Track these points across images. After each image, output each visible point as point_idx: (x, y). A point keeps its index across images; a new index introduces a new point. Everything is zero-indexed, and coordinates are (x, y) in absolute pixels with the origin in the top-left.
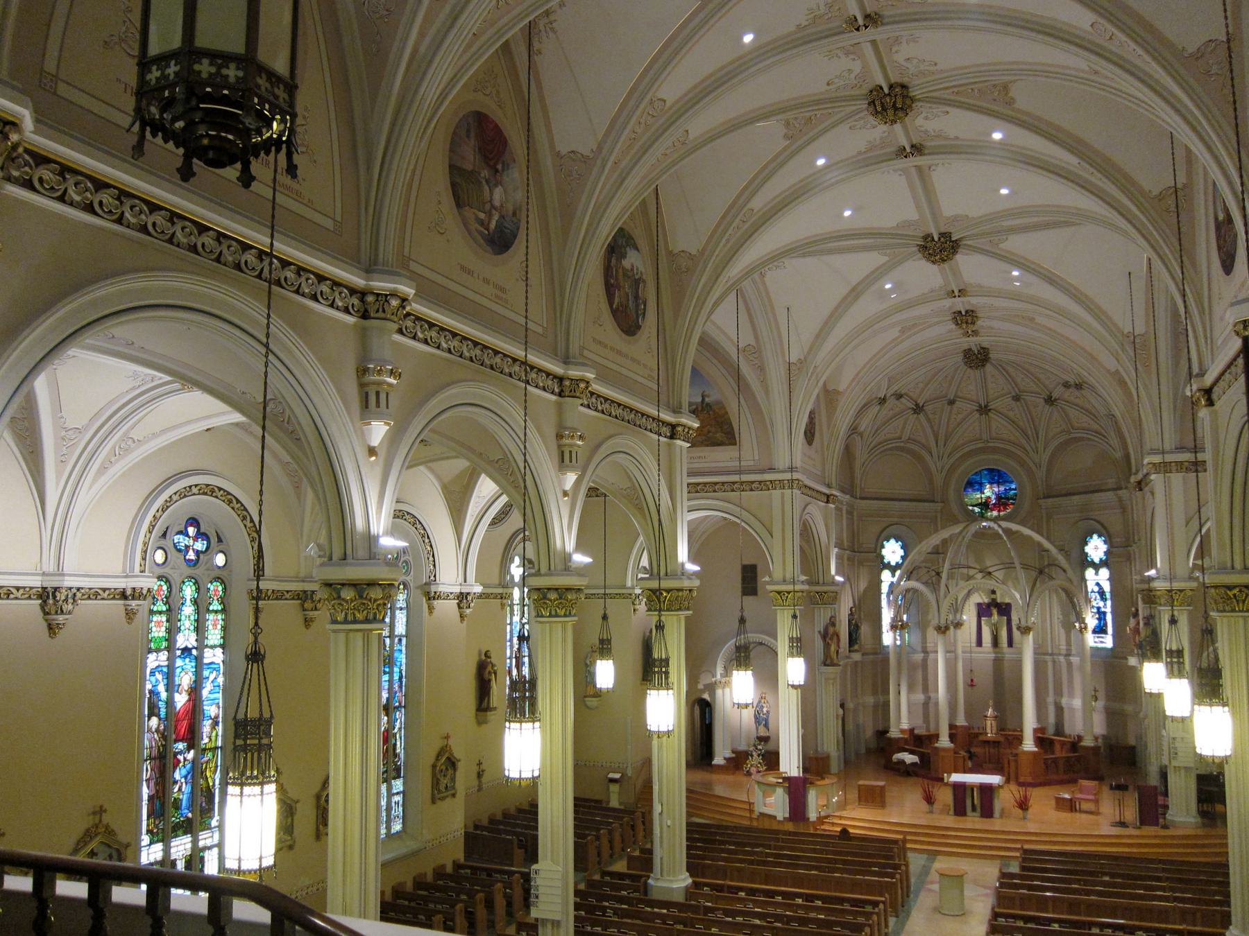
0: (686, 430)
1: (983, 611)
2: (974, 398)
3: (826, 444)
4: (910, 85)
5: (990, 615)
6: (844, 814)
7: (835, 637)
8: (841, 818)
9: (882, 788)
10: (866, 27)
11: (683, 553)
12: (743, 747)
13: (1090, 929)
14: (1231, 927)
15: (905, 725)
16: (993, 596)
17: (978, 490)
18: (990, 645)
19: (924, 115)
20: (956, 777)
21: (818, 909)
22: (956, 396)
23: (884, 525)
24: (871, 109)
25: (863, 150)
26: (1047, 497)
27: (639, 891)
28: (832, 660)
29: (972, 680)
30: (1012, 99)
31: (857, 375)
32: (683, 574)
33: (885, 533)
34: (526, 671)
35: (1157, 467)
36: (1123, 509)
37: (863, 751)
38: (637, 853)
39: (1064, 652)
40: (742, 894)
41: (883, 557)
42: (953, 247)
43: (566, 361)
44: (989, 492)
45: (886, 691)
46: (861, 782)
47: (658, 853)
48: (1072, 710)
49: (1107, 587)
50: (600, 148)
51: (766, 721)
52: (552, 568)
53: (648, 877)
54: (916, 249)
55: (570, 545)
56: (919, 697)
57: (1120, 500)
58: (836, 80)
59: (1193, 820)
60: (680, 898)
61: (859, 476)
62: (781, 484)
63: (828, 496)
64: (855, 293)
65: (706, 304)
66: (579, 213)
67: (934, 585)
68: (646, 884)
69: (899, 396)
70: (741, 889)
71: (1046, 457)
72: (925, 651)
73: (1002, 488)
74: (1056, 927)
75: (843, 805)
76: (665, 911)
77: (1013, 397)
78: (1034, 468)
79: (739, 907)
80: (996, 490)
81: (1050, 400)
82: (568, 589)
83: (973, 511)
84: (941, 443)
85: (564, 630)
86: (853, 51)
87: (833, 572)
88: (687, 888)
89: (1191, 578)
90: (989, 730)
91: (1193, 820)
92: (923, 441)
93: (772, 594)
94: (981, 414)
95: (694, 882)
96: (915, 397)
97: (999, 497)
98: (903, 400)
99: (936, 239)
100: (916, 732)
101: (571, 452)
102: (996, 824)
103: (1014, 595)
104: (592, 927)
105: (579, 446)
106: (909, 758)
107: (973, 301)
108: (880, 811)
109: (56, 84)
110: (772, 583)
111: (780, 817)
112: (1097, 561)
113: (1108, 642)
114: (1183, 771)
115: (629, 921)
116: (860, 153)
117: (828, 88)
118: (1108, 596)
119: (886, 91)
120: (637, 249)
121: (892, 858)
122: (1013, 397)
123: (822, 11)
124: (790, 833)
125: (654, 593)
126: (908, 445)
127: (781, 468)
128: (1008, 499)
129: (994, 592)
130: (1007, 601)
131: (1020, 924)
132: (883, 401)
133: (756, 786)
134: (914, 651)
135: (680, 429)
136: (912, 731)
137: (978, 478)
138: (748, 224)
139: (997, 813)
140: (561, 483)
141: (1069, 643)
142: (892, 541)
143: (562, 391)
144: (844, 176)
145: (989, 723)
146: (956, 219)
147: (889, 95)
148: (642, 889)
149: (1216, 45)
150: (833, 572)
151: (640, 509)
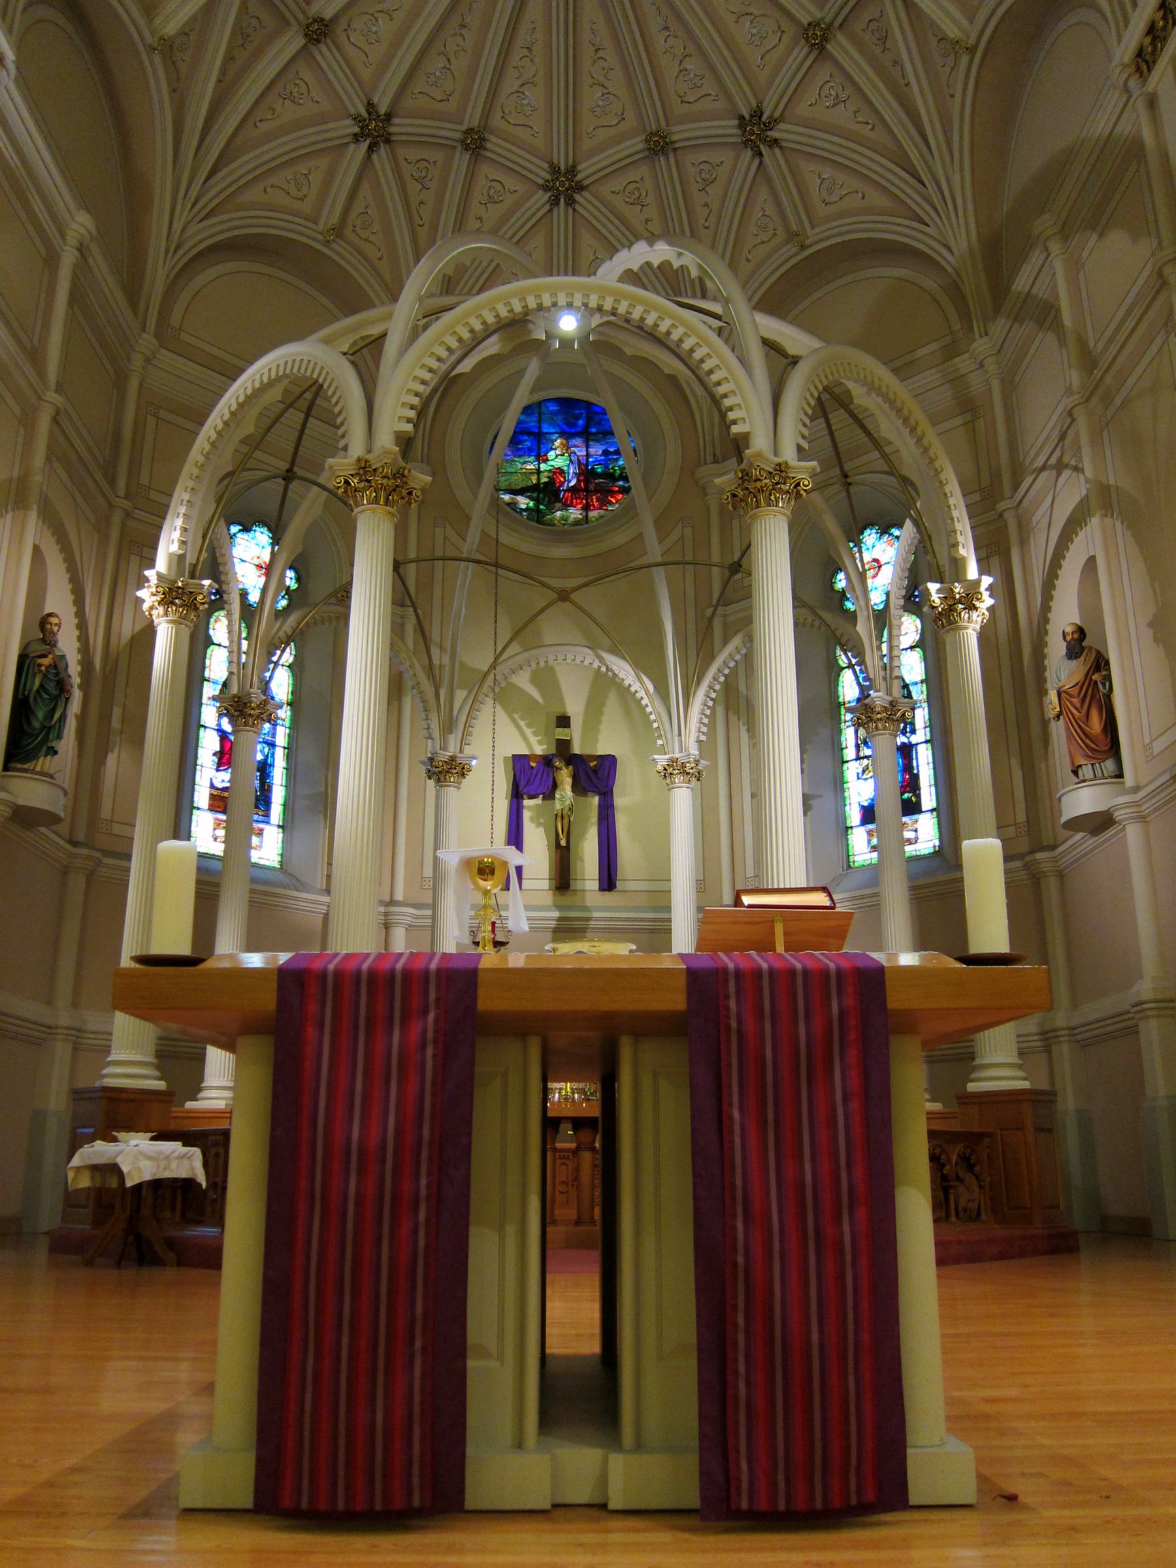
16: (561, 734)
17: (529, 452)
18: (545, 884)
83: (513, 505)
96: (690, 158)
97: (586, 473)
128: (612, 477)
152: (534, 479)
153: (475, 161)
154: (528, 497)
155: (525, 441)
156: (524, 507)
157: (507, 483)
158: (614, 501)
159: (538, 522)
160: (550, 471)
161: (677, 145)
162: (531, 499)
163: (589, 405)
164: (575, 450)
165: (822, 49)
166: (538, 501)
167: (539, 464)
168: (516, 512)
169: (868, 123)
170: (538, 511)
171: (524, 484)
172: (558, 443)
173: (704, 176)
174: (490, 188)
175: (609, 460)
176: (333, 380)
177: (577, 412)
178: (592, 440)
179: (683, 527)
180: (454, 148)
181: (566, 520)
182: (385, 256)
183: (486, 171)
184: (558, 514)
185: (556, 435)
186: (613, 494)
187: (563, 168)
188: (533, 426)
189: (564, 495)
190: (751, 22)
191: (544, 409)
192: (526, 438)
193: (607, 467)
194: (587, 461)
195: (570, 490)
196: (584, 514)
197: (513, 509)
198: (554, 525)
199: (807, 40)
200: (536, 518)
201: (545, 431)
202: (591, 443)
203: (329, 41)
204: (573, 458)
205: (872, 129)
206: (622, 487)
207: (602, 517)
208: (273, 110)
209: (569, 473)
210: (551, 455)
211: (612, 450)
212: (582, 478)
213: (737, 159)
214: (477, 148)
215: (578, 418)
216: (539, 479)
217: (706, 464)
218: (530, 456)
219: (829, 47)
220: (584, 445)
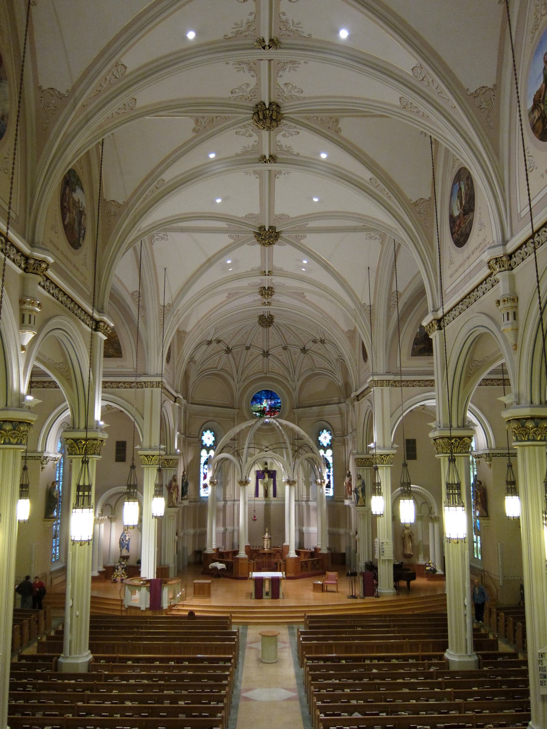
0: (106, 326)
1: (260, 475)
2: (261, 347)
3: (176, 365)
4: (281, 106)
5: (264, 478)
6: (185, 603)
7: (176, 490)
8: (183, 605)
9: (209, 584)
10: (270, 47)
11: (98, 415)
12: (111, 564)
13: (364, 662)
14: (447, 650)
15: (214, 547)
16: (266, 466)
17: (259, 402)
18: (263, 496)
19: (283, 132)
20: (256, 574)
21: (186, 668)
22: (251, 345)
23: (207, 420)
24: (256, 117)
25: (240, 153)
26: (298, 408)
27: (51, 669)
28: (173, 503)
29: (255, 517)
30: (339, 129)
31: (199, 322)
32: (97, 428)
33: (203, 428)
35: (376, 383)
36: (341, 414)
37: (186, 564)
38: (44, 639)
39: (305, 499)
40: (130, 663)
41: (202, 441)
42: (276, 236)
43: (32, 244)
44: (265, 404)
45: (205, 526)
46: (196, 581)
47: (68, 637)
48: (309, 533)
49: (330, 460)
50: (74, 89)
51: (128, 545)
52: (9, 404)
53: (59, 657)
54: (253, 235)
55: (24, 389)
56: (221, 529)
57: (340, 409)
58: (237, 91)
59: (392, 591)
60: (83, 670)
61: (191, 390)
62: (152, 385)
63: (176, 398)
64: (210, 262)
65: (125, 242)
66: (52, 135)
67: (238, 454)
68: (57, 662)
69: (219, 341)
70: (129, 659)
71: (298, 385)
72: (225, 500)
73: (273, 402)
74: (344, 662)
75: (183, 598)
76: (73, 682)
77: (283, 347)
78: (291, 390)
79: (129, 672)
80: (270, 403)
81: (304, 350)
82: (21, 423)
83: (256, 415)
84: (240, 373)
85: (15, 456)
86: (253, 68)
87: (176, 447)
88: (89, 662)
89: (392, 448)
90: (265, 547)
91: (392, 591)
92: (230, 371)
93: (142, 457)
94: (264, 357)
95: (94, 657)
97: (271, 407)
98: (220, 344)
99: (267, 230)
100: (220, 550)
101: (30, 316)
102: (281, 602)
103: (278, 466)
104: (16, 701)
105: (37, 312)
106: (220, 566)
107: (276, 280)
108: (207, 600)
110: (141, 449)
111: (143, 608)
112: (325, 445)
113: (331, 492)
114: (387, 562)
115: (46, 692)
116: (237, 155)
117: (231, 95)
118: (331, 465)
119: (267, 106)
120: (82, 189)
121: (226, 628)
122: (283, 347)
123: (243, 29)
124: (150, 617)
125: (75, 442)
126: (221, 373)
127: (152, 374)
128: (276, 408)
129: (266, 464)
130: (274, 469)
131: (322, 663)
132: (209, 343)
133: (127, 588)
134: (218, 500)
135: (102, 324)
136: (218, 549)
137: (259, 395)
138: (159, 191)
139: (281, 596)
140: (21, 338)
141: (308, 495)
142: (208, 432)
143: (27, 268)
144: (226, 169)
145: (266, 542)
146: (283, 217)
147: (268, 109)
148: (53, 667)
149: (486, 90)
150: (176, 447)
151: (69, 380)
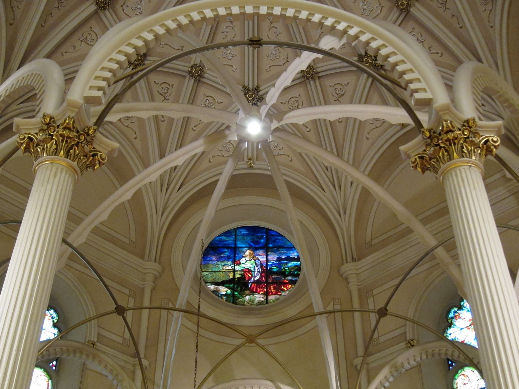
17: (228, 258)
34: (484, 85)
80: (263, 259)
83: (217, 292)
97: (266, 271)
109: (123, 342)
128: (284, 274)
137: (230, 240)
152: (231, 276)
153: (197, 85)
154: (227, 287)
155: (226, 252)
156: (224, 293)
157: (213, 278)
158: (285, 289)
159: (233, 303)
160: (242, 270)
161: (320, 75)
162: (229, 288)
163: (268, 231)
164: (259, 257)
165: (408, 12)
166: (233, 290)
167: (234, 266)
168: (219, 296)
169: (438, 53)
170: (234, 296)
171: (224, 279)
172: (247, 253)
173: (337, 92)
174: (206, 101)
175: (282, 263)
176: (43, 80)
177: (260, 235)
178: (270, 251)
179: (334, 304)
180: (185, 77)
181: (253, 302)
182: (138, 137)
183: (203, 90)
184: (247, 298)
185: (246, 249)
186: (285, 284)
187: (251, 87)
188: (231, 244)
189: (251, 286)
190: (363, 3)
191: (238, 232)
192: (226, 250)
193: (280, 268)
194: (267, 264)
195: (255, 282)
196: (265, 297)
197: (216, 294)
198: (244, 305)
199: (398, 7)
200: (232, 300)
201: (239, 246)
202: (269, 253)
203: (111, 11)
204: (257, 262)
205: (441, 56)
206: (291, 280)
207: (277, 299)
208: (75, 47)
209: (254, 272)
210: (243, 260)
211: (283, 257)
212: (263, 275)
213: (358, 80)
214: (198, 75)
215: (261, 238)
216: (234, 275)
217: (347, 262)
218: (228, 261)
219: (411, 9)
220: (265, 254)
